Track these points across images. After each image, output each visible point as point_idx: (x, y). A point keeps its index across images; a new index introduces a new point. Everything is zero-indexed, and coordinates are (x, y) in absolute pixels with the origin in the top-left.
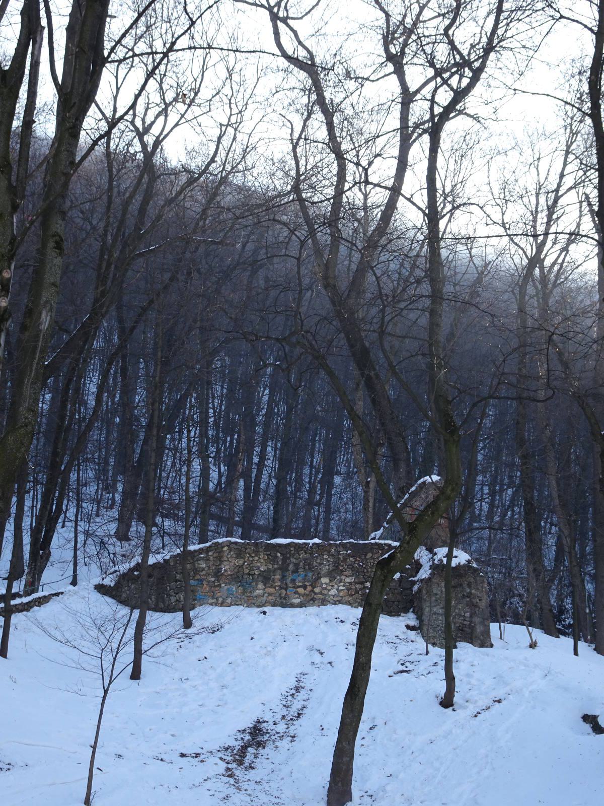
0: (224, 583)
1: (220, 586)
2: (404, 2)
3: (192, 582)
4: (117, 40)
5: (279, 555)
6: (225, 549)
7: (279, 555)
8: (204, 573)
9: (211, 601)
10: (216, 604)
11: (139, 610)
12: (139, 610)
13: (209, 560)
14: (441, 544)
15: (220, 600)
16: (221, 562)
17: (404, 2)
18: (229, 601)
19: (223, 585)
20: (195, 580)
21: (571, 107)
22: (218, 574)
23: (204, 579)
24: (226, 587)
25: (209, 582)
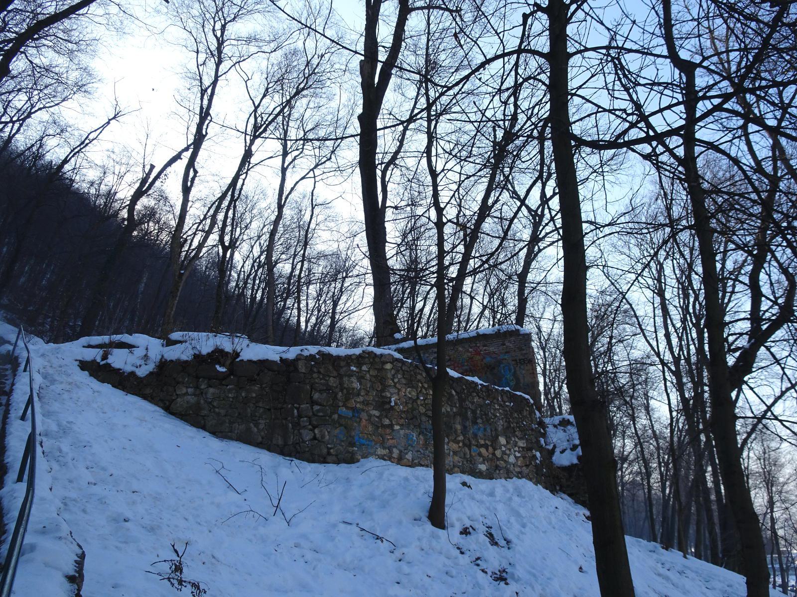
0: (398, 424)
1: (391, 426)
2: (215, 1)
3: (343, 410)
4: (579, 55)
5: (454, 393)
6: (388, 366)
7: (454, 393)
8: (361, 399)
9: (380, 451)
10: (390, 458)
11: (169, 336)
12: (169, 336)
13: (363, 377)
14: (737, 569)
15: (396, 453)
16: (385, 387)
17: (215, 1)
18: (409, 456)
19: (397, 427)
20: (347, 408)
21: (422, 148)
22: (383, 404)
23: (363, 410)
24: (402, 432)
25: (370, 416)
